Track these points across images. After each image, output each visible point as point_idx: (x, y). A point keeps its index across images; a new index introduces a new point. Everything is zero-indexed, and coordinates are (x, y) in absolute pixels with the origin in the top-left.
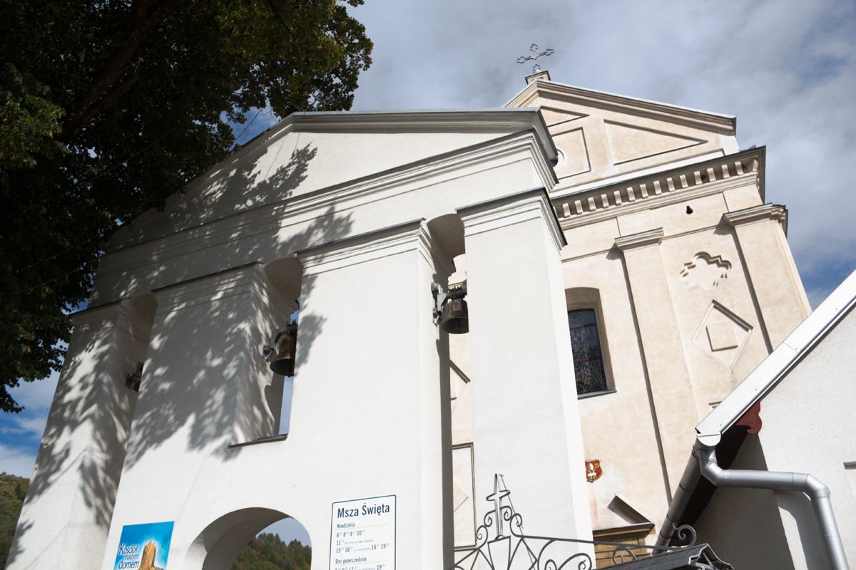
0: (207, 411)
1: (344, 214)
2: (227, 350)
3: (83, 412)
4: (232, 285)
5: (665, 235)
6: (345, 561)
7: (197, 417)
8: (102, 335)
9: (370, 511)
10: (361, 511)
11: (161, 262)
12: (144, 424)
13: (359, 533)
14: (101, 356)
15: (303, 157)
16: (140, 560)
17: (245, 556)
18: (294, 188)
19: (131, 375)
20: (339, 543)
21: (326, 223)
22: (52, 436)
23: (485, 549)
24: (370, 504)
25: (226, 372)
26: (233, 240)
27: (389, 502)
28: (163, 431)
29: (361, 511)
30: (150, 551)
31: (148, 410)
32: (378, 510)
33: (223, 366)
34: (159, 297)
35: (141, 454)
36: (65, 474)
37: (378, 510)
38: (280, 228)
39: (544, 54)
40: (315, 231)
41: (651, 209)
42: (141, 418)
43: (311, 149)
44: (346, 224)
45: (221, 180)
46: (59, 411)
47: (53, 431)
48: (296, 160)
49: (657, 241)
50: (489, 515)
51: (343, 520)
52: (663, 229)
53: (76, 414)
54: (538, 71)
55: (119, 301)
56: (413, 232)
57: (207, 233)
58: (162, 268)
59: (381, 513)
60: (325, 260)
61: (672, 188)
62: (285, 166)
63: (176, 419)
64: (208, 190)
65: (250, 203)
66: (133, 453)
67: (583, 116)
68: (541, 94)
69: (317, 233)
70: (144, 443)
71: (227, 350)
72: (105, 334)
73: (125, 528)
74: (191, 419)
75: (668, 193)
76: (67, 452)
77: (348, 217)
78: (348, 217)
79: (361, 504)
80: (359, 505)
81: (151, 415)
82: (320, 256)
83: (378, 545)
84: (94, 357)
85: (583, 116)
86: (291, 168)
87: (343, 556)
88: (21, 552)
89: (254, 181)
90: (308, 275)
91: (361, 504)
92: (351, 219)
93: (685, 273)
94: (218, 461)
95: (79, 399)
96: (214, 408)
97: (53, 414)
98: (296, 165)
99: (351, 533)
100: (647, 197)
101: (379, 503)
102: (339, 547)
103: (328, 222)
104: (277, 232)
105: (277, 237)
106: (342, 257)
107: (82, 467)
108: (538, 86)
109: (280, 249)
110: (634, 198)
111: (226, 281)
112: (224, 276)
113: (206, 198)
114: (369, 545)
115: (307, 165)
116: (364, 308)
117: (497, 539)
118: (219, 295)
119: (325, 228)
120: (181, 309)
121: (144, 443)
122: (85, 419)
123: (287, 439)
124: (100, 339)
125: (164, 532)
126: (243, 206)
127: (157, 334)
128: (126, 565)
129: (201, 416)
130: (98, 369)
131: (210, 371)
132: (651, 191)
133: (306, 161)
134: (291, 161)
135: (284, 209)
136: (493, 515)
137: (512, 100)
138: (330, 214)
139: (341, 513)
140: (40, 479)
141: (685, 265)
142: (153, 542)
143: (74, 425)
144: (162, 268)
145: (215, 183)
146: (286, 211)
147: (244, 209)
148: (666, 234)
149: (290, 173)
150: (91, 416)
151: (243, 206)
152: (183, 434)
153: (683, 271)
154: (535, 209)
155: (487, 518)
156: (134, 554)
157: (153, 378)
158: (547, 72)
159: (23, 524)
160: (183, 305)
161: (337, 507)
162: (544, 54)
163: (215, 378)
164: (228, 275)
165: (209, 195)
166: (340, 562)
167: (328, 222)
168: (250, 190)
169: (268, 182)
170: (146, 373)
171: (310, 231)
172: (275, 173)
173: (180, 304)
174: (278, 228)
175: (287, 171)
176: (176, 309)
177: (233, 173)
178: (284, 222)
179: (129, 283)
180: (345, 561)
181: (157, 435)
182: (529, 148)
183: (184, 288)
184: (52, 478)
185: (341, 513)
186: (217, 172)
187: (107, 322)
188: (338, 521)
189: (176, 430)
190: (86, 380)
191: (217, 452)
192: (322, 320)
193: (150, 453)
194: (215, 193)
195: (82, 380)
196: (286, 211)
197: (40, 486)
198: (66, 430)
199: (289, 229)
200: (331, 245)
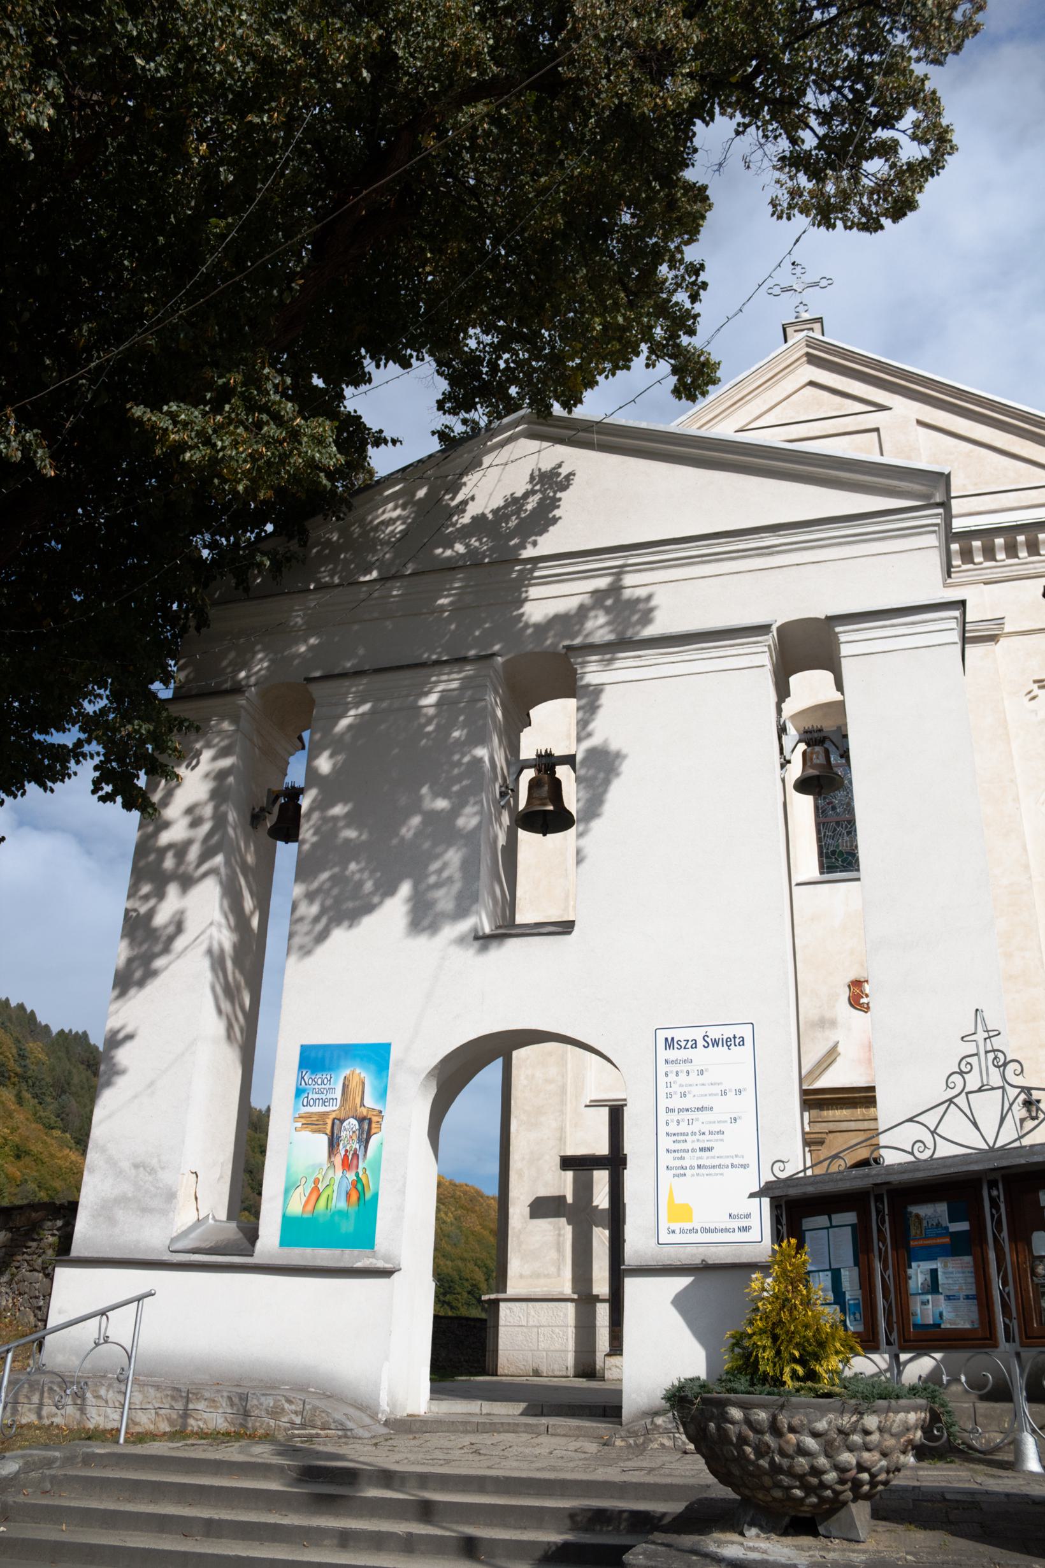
0: (432, 879)
1: (642, 593)
2: (456, 788)
3: (199, 865)
4: (455, 685)
5: (1006, 631)
6: (680, 1110)
7: (415, 887)
8: (216, 740)
9: (715, 1043)
10: (701, 1043)
11: (312, 628)
12: (319, 890)
13: (701, 1073)
14: (221, 776)
15: (551, 483)
16: (338, 1094)
17: (82, 1088)
18: (540, 534)
19: (257, 810)
20: (668, 1085)
21: (609, 602)
22: (146, 898)
23: (961, 1101)
24: (714, 1033)
25: (461, 822)
26: (442, 608)
27: (745, 1031)
28: (357, 903)
29: (701, 1043)
30: (354, 1084)
31: (325, 870)
32: (728, 1042)
33: (455, 812)
34: (316, 690)
35: (322, 937)
36: (180, 961)
37: (728, 1042)
38: (526, 600)
39: (816, 284)
40: (592, 614)
41: (985, 584)
42: (312, 882)
43: (564, 471)
44: (643, 610)
45: (400, 502)
46: (152, 857)
47: (146, 889)
48: (538, 487)
49: (993, 639)
50: (968, 1060)
51: (673, 1054)
52: (1005, 621)
53: (189, 864)
54: (806, 316)
55: (238, 689)
56: (759, 639)
57: (395, 593)
58: (313, 641)
59: (733, 1047)
60: (618, 664)
61: (1023, 553)
62: (519, 494)
63: (377, 887)
64: (378, 517)
65: (460, 548)
66: (307, 933)
67: (882, 408)
68: (812, 360)
69: (596, 617)
70: (324, 921)
71: (456, 788)
72: (222, 740)
73: (305, 1050)
74: (405, 889)
75: (1016, 561)
76: (179, 926)
77: (649, 597)
78: (649, 597)
79: (701, 1032)
80: (698, 1034)
81: (331, 878)
82: (608, 656)
83: (730, 1090)
84: (207, 775)
85: (882, 408)
86: (530, 500)
87: (677, 1102)
88: (122, 1072)
89: (464, 511)
90: (588, 685)
91: (701, 1032)
92: (653, 603)
93: (1032, 695)
94: (468, 955)
95: (188, 843)
96: (445, 874)
97: (142, 863)
98: (538, 496)
99: (688, 1072)
100: (981, 563)
101: (728, 1032)
102: (669, 1090)
103: (611, 599)
104: (521, 606)
105: (522, 615)
106: (643, 663)
107: (210, 952)
108: (808, 346)
109: (531, 635)
110: (959, 563)
111: (445, 677)
112: (437, 669)
113: (376, 529)
114: (717, 1089)
115: (560, 499)
116: (679, 741)
117: (980, 1090)
118: (432, 699)
119: (608, 611)
120: (363, 714)
121: (324, 921)
122: (205, 875)
123: (574, 933)
124: (214, 746)
125: (377, 1056)
126: (449, 553)
127: (325, 749)
128: (315, 1103)
129: (423, 886)
130: (218, 795)
131: (431, 817)
132: (989, 553)
133: (555, 493)
134: (529, 487)
135: (532, 571)
136: (974, 1060)
137: (762, 363)
138: (616, 589)
139: (670, 1043)
140: (135, 964)
141: (1035, 682)
142: (358, 1071)
143: (187, 882)
144: (313, 641)
145: (391, 505)
146: (536, 574)
147: (449, 558)
148: (1008, 629)
149: (529, 507)
150: (213, 871)
151: (449, 553)
152: (394, 910)
153: (1030, 692)
154: (946, 627)
155: (964, 1062)
156: (327, 1086)
157: (325, 820)
158: (820, 320)
159: (118, 1031)
160: (366, 708)
161: (662, 1035)
162: (816, 284)
163: (442, 829)
164: (447, 670)
165: (382, 523)
166: (672, 1110)
167: (611, 599)
168: (458, 526)
169: (490, 516)
170: (311, 810)
171: (582, 612)
172: (502, 503)
173: (357, 705)
174: (522, 602)
175: (523, 505)
176: (352, 712)
177: (421, 493)
178: (534, 592)
179: (253, 657)
180: (680, 1110)
181: (345, 908)
182: (934, 532)
183: (365, 681)
184: (159, 963)
185: (670, 1043)
186: (397, 488)
187: (222, 718)
188: (664, 1054)
189: (381, 903)
190: (197, 812)
191: (461, 941)
192: (619, 756)
193: (339, 936)
194: (392, 521)
195: (189, 811)
196: (536, 574)
197: (138, 974)
198: (172, 890)
199: (542, 604)
200: (624, 644)
